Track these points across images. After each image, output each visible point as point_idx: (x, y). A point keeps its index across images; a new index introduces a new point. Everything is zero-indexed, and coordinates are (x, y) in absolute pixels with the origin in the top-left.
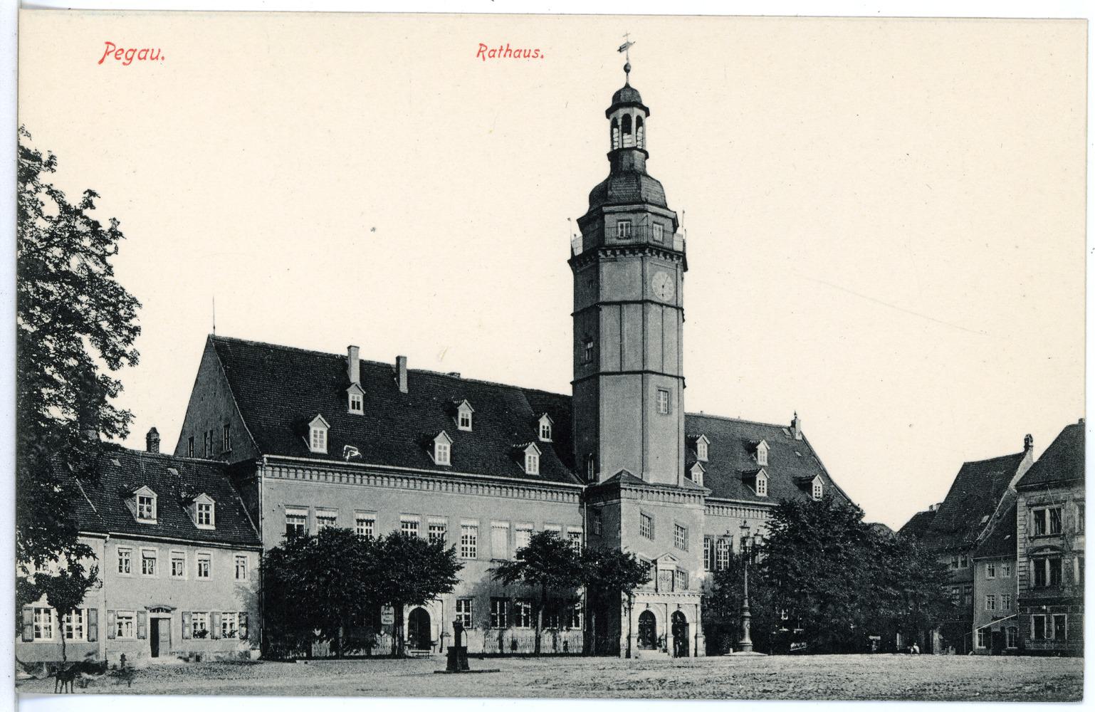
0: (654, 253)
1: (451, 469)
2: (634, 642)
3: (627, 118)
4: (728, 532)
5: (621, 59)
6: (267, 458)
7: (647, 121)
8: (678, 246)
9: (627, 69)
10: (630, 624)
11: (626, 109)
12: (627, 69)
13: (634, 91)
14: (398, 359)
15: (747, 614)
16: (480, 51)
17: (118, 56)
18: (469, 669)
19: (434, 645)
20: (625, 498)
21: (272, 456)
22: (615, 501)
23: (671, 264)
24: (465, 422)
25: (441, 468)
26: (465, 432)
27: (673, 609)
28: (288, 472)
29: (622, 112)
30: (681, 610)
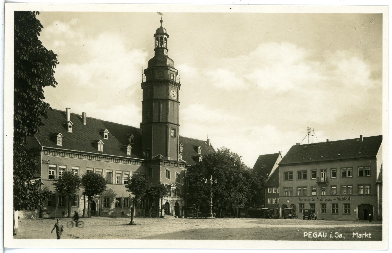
0: (171, 83)
1: (103, 153)
3: (162, 38)
6: (43, 147)
7: (168, 39)
8: (177, 81)
9: (161, 21)
11: (160, 35)
12: (161, 21)
14: (83, 113)
15: (212, 205)
18: (15, 211)
19: (97, 213)
20: (161, 165)
21: (45, 147)
22: (157, 165)
23: (176, 88)
24: (106, 136)
25: (100, 152)
26: (106, 140)
28: (47, 152)
29: (160, 36)
30: (168, 202)
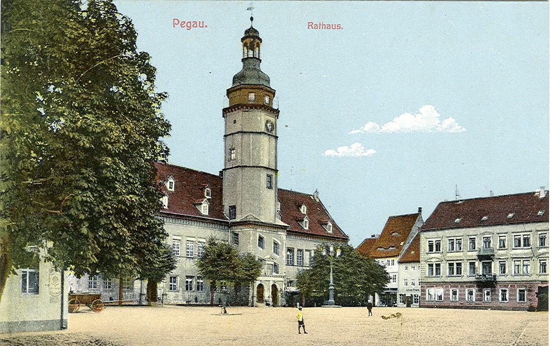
2: (255, 299)
4: (52, 270)
5: (249, 14)
9: (252, 19)
10: (253, 291)
11: (252, 39)
13: (256, 31)
16: (309, 26)
17: (183, 26)
27: (272, 283)
